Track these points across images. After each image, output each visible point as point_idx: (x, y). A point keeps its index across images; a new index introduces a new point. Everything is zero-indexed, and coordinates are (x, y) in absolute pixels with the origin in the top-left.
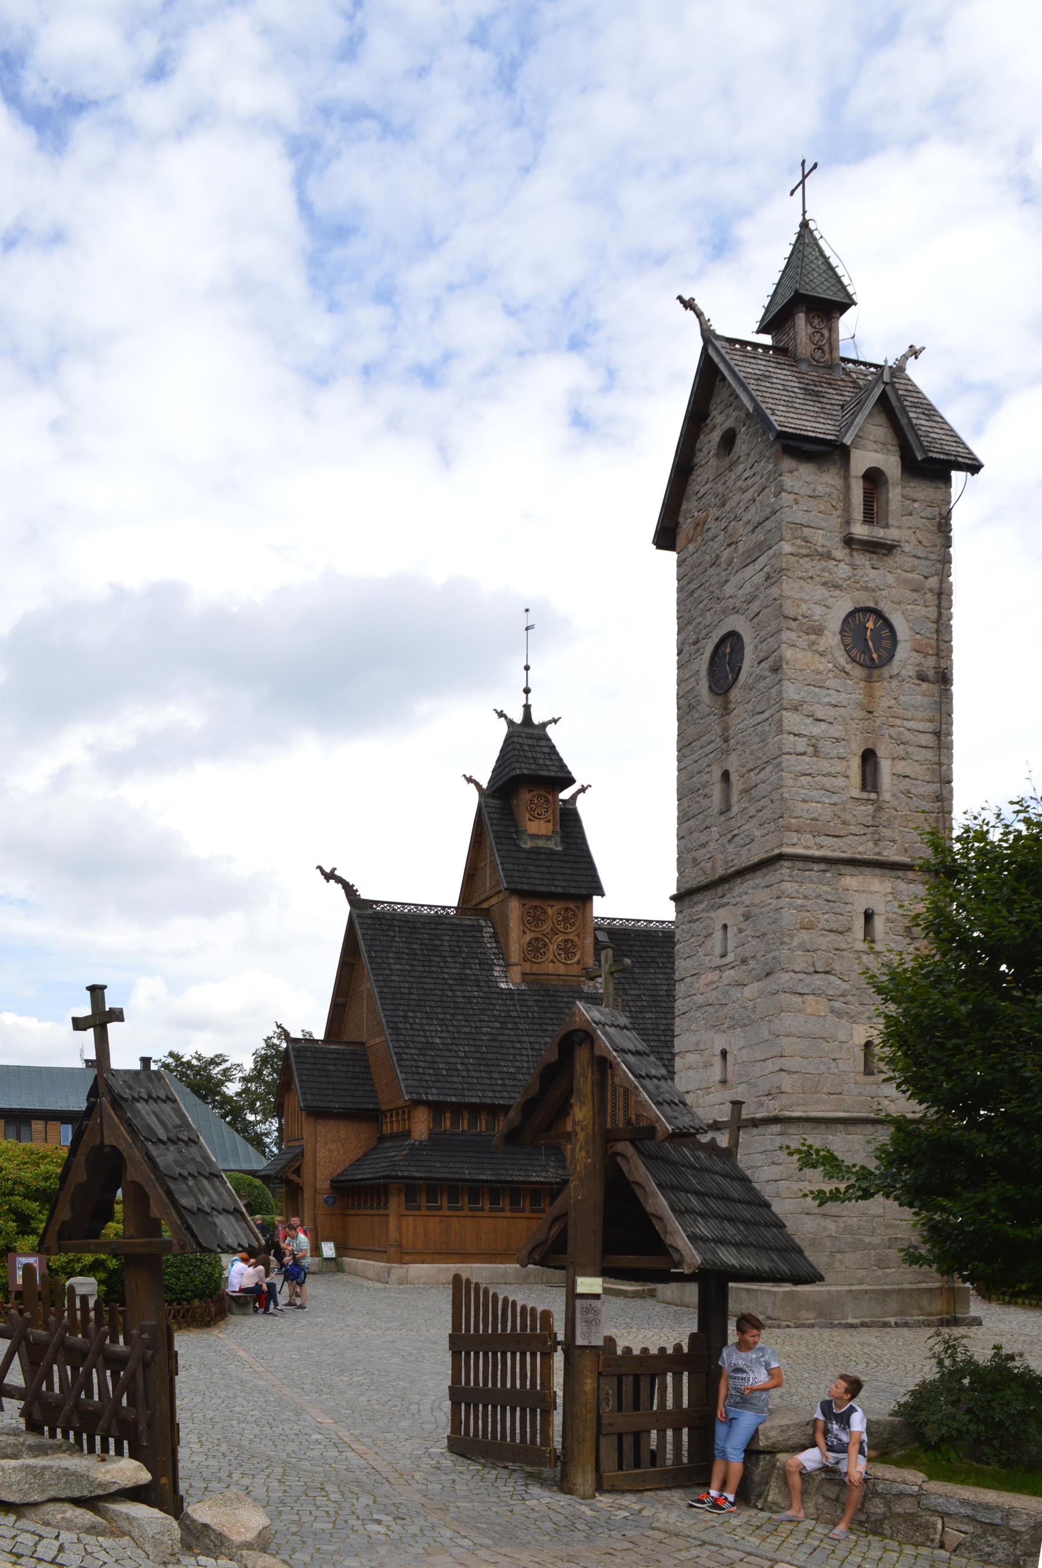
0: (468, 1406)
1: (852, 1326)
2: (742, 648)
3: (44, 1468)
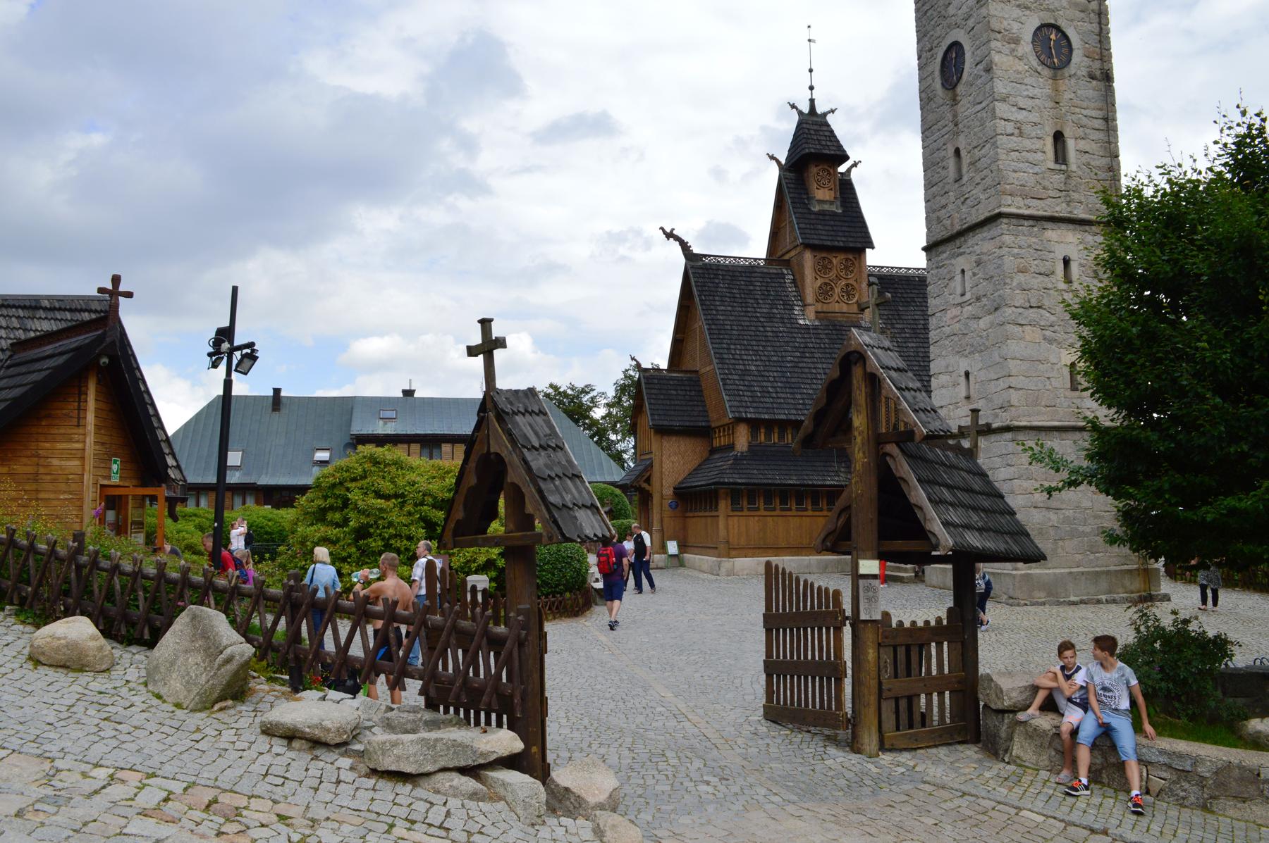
0: (778, 677)
1: (1073, 603)
2: (964, 53)
3: (436, 740)
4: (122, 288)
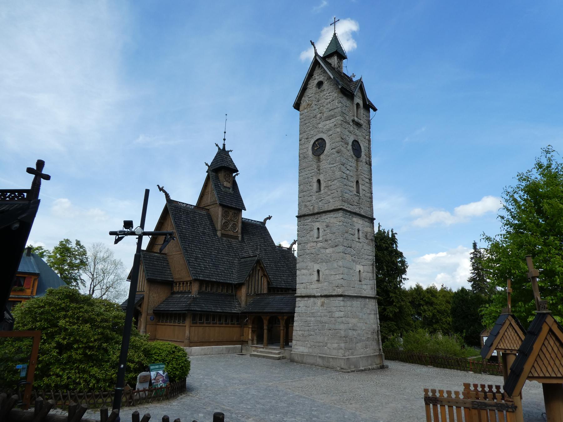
4: (44, 171)
